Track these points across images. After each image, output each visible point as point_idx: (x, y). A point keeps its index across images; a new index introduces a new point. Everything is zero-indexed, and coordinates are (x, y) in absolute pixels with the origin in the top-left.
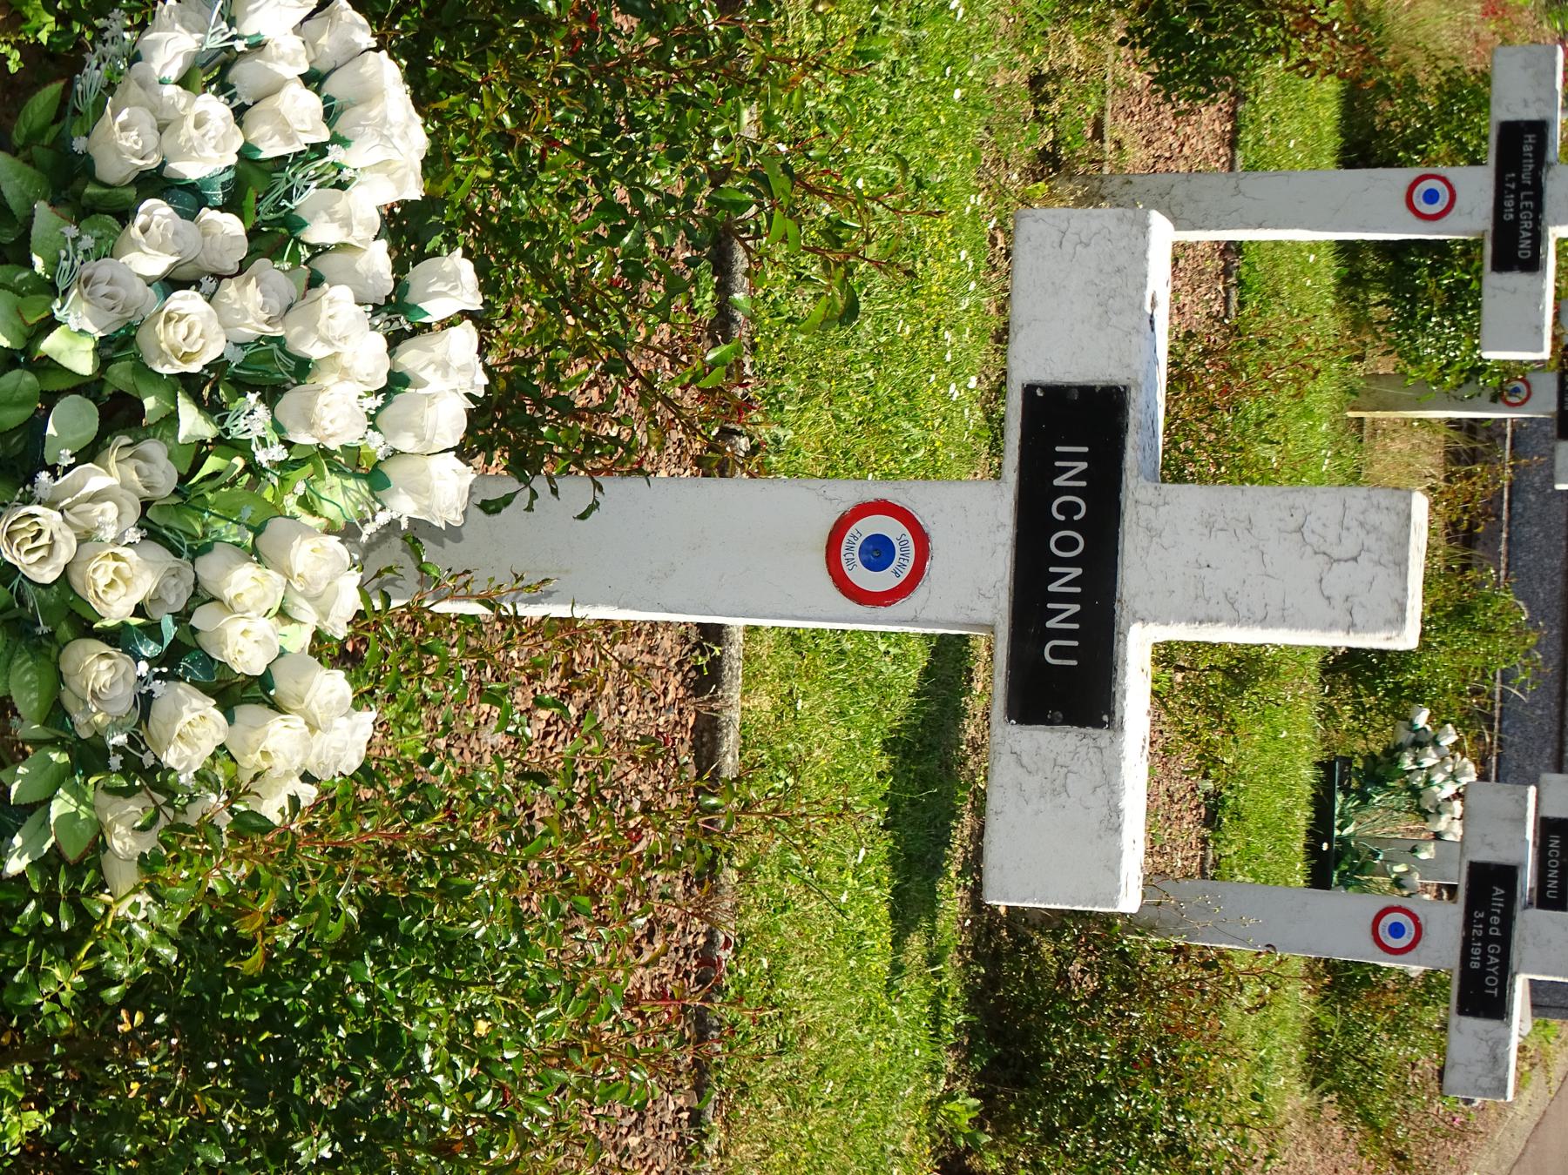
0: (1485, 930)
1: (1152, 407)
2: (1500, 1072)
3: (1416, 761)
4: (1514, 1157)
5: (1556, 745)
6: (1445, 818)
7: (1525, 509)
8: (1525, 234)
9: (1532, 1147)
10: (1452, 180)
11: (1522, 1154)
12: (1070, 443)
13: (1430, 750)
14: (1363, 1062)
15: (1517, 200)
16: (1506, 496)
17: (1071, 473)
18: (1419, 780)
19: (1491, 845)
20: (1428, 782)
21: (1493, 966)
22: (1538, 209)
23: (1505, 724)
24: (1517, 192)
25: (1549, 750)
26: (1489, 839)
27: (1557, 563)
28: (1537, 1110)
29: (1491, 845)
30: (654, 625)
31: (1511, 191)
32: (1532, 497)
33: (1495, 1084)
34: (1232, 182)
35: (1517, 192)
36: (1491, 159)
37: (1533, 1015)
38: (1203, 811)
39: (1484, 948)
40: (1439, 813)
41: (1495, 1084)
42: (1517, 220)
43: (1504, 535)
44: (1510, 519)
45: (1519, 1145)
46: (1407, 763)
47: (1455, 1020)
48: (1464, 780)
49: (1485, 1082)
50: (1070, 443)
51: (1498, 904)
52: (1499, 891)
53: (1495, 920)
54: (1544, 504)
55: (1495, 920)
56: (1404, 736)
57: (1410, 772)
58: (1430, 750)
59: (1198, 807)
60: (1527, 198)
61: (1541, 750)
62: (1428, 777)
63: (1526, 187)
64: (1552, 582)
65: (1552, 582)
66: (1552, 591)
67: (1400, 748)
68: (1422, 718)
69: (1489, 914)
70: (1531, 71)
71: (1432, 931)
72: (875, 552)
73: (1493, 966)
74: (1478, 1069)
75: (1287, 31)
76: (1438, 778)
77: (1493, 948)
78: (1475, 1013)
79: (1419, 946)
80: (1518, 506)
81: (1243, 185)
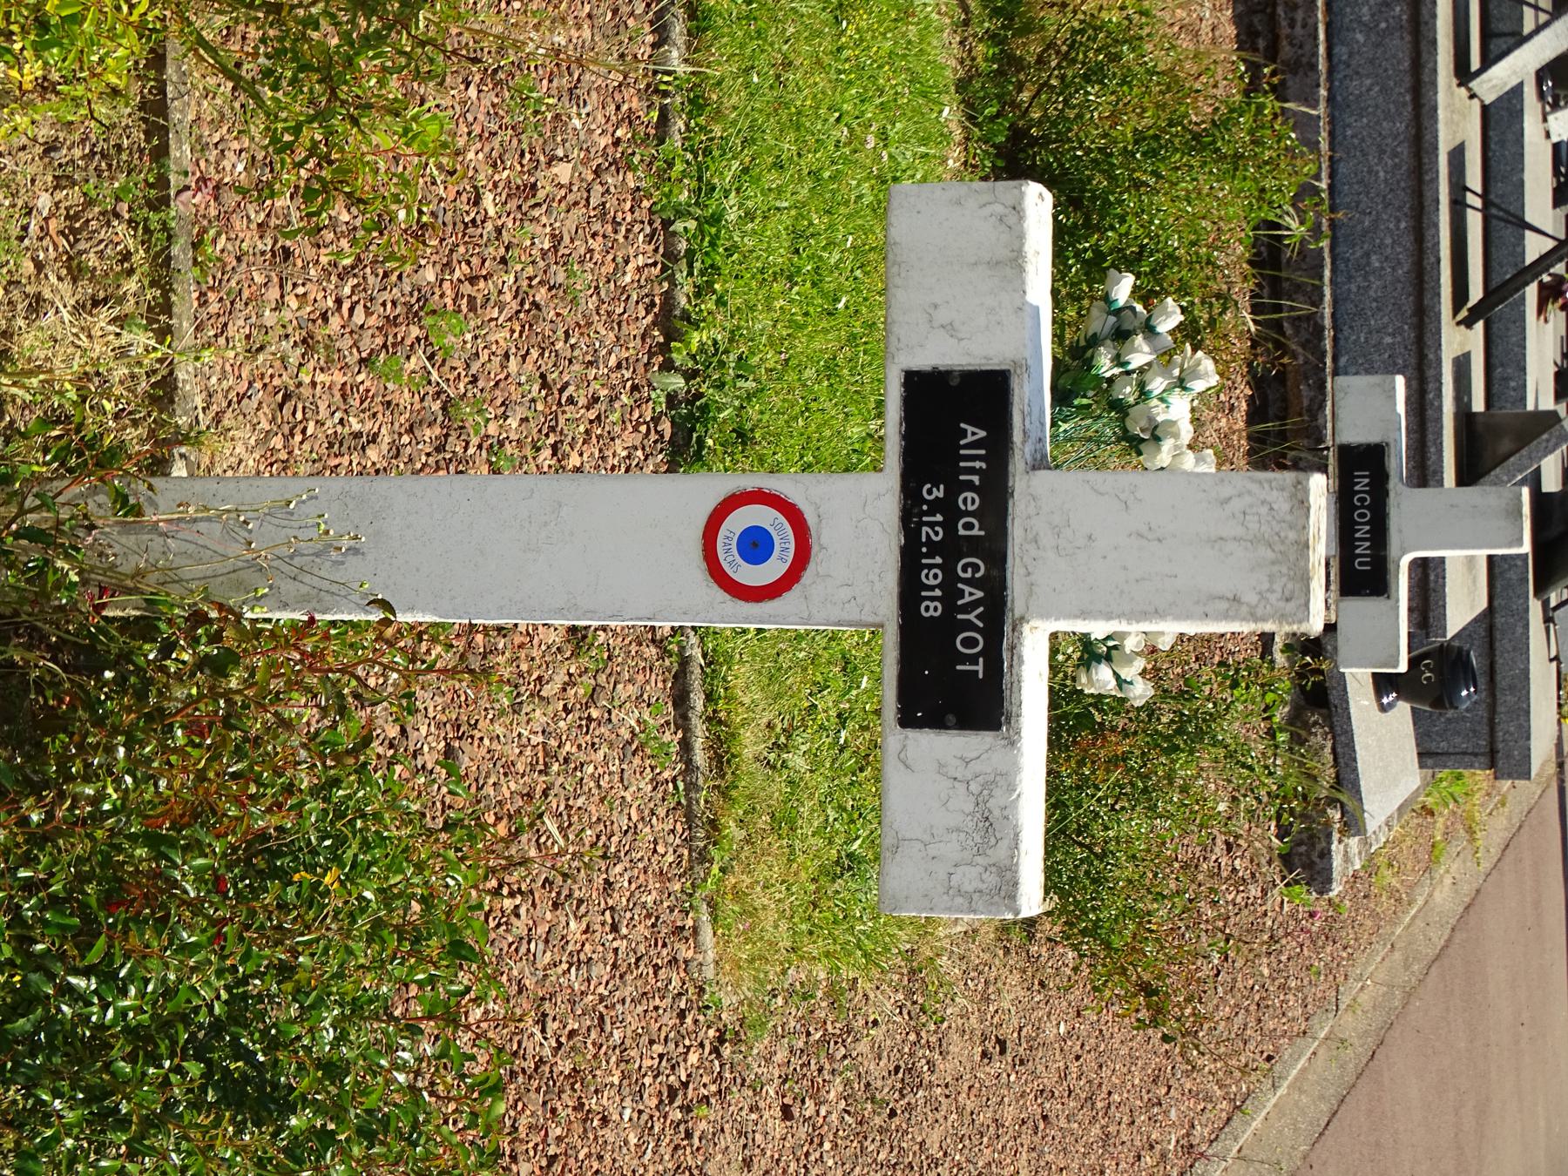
0: (949, 526)
1: (1034, 397)
2: (1000, 853)
3: (1118, 361)
4: (1432, 953)
6: (1167, 445)
7: (1351, 55)
9: (1459, 937)
11: (1446, 947)
12: (954, 424)
13: (1139, 339)
14: (1089, 848)
16: (1322, 36)
17: (1362, 484)
18: (1127, 392)
19: (949, 328)
20: (1143, 394)
21: (969, 608)
23: (1343, 361)
26: (942, 316)
27: (1400, 127)
28: (1467, 889)
29: (949, 328)
32: (1360, 37)
33: (991, 879)
37: (1421, 767)
38: (666, 427)
39: (948, 569)
40: (1157, 439)
41: (991, 879)
43: (1323, 92)
44: (1331, 71)
45: (1438, 937)
46: (1104, 365)
47: (896, 739)
48: (1198, 386)
49: (968, 878)
50: (954, 424)
51: (974, 466)
52: (974, 433)
53: (969, 500)
54: (1377, 45)
55: (969, 500)
56: (1099, 322)
57: (1110, 381)
58: (1139, 339)
59: (656, 420)
62: (1141, 386)
64: (1395, 155)
65: (1395, 155)
67: (1094, 341)
68: (1123, 288)
69: (955, 488)
71: (827, 537)
72: (757, 552)
73: (969, 608)
74: (950, 849)
76: (1157, 385)
77: (970, 566)
78: (935, 721)
79: (808, 576)
80: (1341, 51)
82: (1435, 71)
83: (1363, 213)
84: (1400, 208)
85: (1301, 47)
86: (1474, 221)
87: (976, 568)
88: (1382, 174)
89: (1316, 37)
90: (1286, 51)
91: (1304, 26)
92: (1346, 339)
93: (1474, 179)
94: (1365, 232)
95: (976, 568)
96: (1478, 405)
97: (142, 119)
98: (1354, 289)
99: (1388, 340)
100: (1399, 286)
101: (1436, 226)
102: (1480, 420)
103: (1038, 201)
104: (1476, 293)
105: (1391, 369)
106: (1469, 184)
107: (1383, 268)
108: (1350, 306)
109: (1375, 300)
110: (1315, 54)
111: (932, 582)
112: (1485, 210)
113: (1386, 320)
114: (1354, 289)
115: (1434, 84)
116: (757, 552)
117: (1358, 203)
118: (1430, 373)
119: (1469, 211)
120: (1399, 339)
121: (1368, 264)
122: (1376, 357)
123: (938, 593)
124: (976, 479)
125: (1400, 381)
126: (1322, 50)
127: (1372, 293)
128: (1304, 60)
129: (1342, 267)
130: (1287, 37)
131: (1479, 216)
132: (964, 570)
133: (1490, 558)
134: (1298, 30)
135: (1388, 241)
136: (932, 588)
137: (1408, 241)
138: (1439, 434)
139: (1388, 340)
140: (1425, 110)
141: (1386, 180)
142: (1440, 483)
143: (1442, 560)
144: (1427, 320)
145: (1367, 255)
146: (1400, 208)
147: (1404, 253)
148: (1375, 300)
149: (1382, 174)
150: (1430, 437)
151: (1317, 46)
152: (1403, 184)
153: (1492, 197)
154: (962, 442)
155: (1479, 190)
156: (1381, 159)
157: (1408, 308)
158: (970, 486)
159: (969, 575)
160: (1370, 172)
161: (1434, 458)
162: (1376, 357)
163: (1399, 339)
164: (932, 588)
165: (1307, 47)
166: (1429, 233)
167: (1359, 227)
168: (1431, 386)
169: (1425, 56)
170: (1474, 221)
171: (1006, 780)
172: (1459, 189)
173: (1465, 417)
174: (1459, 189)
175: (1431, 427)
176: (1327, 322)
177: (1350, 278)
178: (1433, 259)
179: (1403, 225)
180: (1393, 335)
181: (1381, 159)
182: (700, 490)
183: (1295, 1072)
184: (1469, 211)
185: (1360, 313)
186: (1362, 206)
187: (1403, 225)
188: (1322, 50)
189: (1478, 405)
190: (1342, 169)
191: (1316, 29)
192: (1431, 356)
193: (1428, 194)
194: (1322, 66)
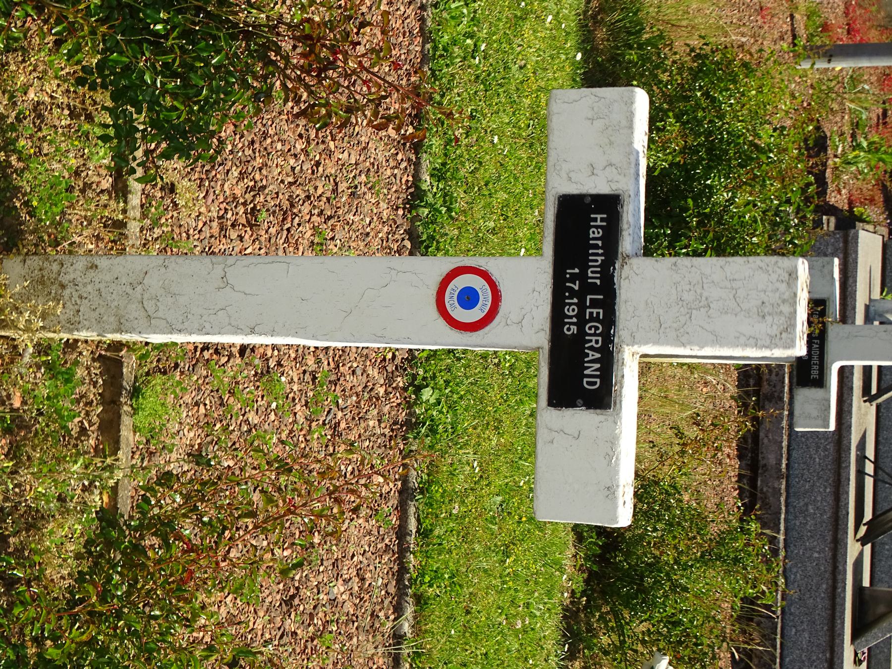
5: (830, 582)
8: (594, 355)
10: (496, 276)
12: (582, 231)
15: (582, 306)
22: (610, 320)
24: (581, 295)
25: (824, 586)
30: (316, 348)
31: (573, 293)
34: (218, 271)
35: (581, 295)
36: (548, 248)
42: (582, 332)
50: (582, 231)
60: (595, 304)
61: (818, 586)
63: (594, 289)
64: (826, 450)
65: (826, 450)
66: (826, 456)
70: (599, 124)
72: (469, 301)
75: (308, 143)
81: (233, 275)
82: (851, 405)
83: (806, 481)
84: (827, 481)
85: (774, 387)
86: (869, 482)
87: (597, 328)
88: (817, 460)
89: (783, 382)
90: (766, 389)
91: (777, 375)
92: (792, 552)
93: (870, 453)
94: (806, 492)
95: (597, 328)
96: (866, 583)
97: (16, 507)
98: (798, 524)
99: (816, 555)
100: (824, 525)
101: (847, 493)
102: (867, 592)
103: (641, 100)
104: (868, 516)
105: (834, 255)
106: (867, 455)
107: (815, 514)
108: (795, 533)
109: (810, 531)
110: (783, 392)
111: (571, 313)
112: (875, 476)
113: (815, 543)
114: (798, 524)
115: (850, 412)
116: (469, 301)
117: (803, 475)
118: (840, 577)
119: (867, 477)
120: (822, 555)
121: (807, 510)
122: (808, 564)
123: (575, 320)
124: (600, 243)
125: (836, 261)
126: (786, 389)
127: (808, 527)
128: (776, 394)
129: (792, 510)
130: (767, 380)
131: (872, 479)
132: (590, 328)
133: (879, 367)
134: (773, 377)
135: (819, 498)
136: (571, 317)
137: (830, 499)
138: (843, 613)
139: (816, 555)
140: (844, 427)
141: (819, 464)
142: (853, 322)
143: (853, 366)
144: (839, 547)
145: (806, 505)
146: (827, 481)
147: (827, 506)
148: (810, 531)
149: (817, 460)
150: (838, 614)
151: (784, 387)
152: (829, 467)
153: (881, 465)
154: (586, 359)
155: (872, 459)
156: (817, 451)
157: (829, 538)
158: (596, 247)
159: (593, 331)
160: (811, 458)
161: (839, 626)
162: (808, 564)
163: (822, 555)
164: (571, 317)
165: (778, 388)
166: (843, 497)
167: (803, 489)
168: (840, 585)
169: (845, 396)
170: (869, 482)
171: (613, 442)
172: (861, 473)
173: (858, 589)
174: (861, 473)
175: (838, 608)
176: (783, 491)
177: (796, 517)
178: (844, 512)
179: (828, 490)
180: (819, 553)
181: (817, 451)
182: (434, 267)
183: (761, 648)
184: (867, 477)
185: (801, 538)
186: (805, 476)
187: (828, 490)
188: (786, 389)
189: (866, 583)
190: (794, 454)
191: (784, 378)
192: (841, 568)
193: (844, 475)
194: (786, 399)
